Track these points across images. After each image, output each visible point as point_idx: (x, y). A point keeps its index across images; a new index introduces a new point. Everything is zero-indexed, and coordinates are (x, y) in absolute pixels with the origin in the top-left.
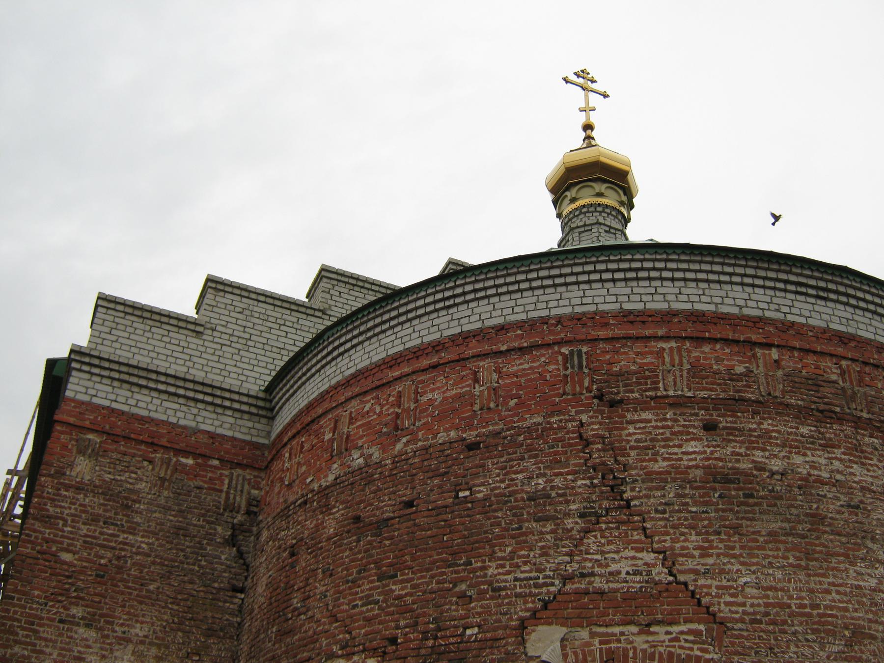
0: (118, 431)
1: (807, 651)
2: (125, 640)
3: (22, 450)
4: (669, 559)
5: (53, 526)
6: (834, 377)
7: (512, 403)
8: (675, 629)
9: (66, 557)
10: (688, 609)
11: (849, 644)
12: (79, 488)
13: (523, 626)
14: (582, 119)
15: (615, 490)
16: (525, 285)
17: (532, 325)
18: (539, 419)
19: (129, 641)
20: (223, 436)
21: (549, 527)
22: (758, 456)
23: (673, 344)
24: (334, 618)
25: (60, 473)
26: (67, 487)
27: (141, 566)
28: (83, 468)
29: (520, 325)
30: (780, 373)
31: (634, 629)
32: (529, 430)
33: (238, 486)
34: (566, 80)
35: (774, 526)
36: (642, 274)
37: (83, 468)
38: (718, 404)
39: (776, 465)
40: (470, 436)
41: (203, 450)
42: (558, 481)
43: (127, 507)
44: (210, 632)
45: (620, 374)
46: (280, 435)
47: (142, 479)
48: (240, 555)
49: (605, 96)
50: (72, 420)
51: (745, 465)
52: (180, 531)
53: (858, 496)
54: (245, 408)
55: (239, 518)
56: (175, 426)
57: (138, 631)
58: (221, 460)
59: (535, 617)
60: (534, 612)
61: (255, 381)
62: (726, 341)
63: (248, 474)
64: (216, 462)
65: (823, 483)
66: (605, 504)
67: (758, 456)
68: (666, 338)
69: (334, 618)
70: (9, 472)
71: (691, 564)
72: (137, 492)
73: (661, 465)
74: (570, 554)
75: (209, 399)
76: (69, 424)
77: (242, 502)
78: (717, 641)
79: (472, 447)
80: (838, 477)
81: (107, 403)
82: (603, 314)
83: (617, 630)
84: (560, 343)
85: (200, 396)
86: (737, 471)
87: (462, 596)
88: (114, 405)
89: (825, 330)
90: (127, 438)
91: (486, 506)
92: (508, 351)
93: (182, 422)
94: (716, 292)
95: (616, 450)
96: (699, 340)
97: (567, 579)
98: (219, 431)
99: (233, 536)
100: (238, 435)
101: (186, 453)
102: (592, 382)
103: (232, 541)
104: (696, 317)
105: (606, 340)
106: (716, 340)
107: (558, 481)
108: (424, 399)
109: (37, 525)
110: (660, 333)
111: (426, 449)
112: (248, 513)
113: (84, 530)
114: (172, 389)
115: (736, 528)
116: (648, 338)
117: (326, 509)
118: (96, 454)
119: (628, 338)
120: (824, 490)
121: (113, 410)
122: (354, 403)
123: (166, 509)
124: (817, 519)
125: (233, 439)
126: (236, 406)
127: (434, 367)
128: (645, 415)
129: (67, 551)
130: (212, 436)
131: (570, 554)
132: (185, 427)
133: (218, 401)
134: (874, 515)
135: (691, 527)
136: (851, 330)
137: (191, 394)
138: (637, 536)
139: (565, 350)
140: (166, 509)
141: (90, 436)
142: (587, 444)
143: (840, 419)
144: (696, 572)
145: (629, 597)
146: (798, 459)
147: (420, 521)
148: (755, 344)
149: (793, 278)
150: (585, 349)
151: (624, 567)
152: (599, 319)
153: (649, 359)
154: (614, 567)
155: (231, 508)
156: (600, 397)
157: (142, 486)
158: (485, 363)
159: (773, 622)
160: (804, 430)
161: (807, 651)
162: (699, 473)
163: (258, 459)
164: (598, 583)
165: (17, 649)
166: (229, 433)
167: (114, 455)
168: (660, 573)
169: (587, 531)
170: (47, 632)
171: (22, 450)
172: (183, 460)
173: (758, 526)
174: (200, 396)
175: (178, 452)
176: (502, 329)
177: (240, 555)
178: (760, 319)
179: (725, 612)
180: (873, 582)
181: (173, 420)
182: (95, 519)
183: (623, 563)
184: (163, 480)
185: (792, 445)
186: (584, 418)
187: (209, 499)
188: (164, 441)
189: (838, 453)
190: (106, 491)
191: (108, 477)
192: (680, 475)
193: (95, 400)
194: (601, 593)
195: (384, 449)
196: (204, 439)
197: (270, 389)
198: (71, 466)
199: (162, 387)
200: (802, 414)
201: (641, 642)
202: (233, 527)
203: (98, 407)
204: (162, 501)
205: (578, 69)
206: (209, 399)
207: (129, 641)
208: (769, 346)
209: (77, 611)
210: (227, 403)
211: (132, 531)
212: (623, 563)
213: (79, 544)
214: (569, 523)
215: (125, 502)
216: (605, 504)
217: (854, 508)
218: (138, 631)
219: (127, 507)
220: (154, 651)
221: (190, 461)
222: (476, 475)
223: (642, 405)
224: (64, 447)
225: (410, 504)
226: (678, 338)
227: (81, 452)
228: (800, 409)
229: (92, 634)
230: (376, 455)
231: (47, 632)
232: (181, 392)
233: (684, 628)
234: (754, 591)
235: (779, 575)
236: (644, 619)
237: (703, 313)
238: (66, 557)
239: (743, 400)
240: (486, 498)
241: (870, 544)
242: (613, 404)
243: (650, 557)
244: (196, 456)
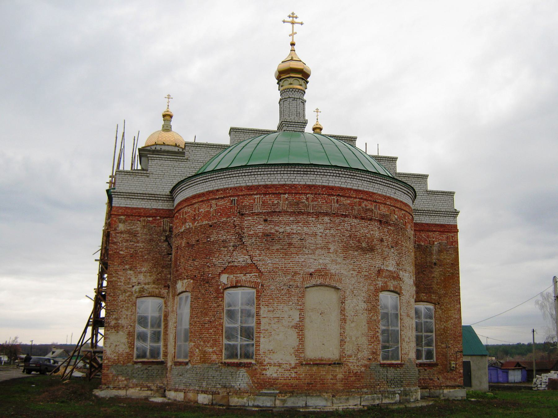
0: (129, 214)
1: (282, 279)
2: (141, 272)
3: (113, 167)
4: (251, 257)
5: (116, 245)
6: (304, 201)
7: (219, 214)
8: (251, 275)
9: (121, 252)
10: (254, 270)
11: (293, 276)
12: (121, 233)
13: (220, 274)
14: (290, 40)
15: (241, 239)
16: (223, 177)
17: (225, 190)
18: (225, 219)
19: (142, 272)
20: (159, 209)
21: (226, 249)
22: (277, 228)
23: (258, 196)
24: (185, 270)
25: (115, 229)
26: (118, 233)
27: (142, 252)
28: (121, 227)
29: (222, 190)
30: (287, 202)
31: (242, 275)
32: (223, 222)
33: (165, 223)
34: (284, 22)
35: (278, 247)
36: (252, 173)
37: (121, 227)
38: (268, 213)
39: (281, 230)
40: (210, 223)
41: (154, 215)
42: (228, 237)
43: (136, 236)
44: (163, 267)
45: (244, 206)
46: (179, 204)
47: (138, 226)
48: (169, 244)
49: (302, 24)
50: (116, 213)
51: (273, 231)
52: (151, 240)
53: (304, 236)
54: (165, 199)
55: (167, 233)
56: (145, 209)
57: (144, 269)
58: (160, 217)
59: (222, 272)
60: (222, 271)
61: (167, 191)
62: (273, 194)
63: (168, 220)
64: (159, 218)
65: (294, 234)
66: (238, 243)
67: (277, 228)
68: (257, 194)
69: (185, 270)
70: (110, 177)
71: (256, 258)
72: (137, 231)
73: (252, 232)
74: (230, 256)
75: (154, 198)
76: (115, 215)
77: (168, 228)
78: (260, 277)
79: (211, 226)
80: (299, 231)
81: (124, 206)
82: (241, 187)
83: (239, 275)
84: (231, 196)
85: (151, 198)
86: (271, 233)
87: (208, 266)
88: (127, 206)
89: (305, 185)
90: (132, 215)
91: (213, 243)
92: (219, 198)
93: (147, 207)
94: (272, 177)
95: (242, 228)
96: (265, 194)
97: (229, 263)
98: (159, 208)
99: (166, 239)
100: (164, 208)
101: (150, 217)
102: (237, 208)
103: (166, 240)
104: (266, 186)
105: (242, 195)
106: (269, 194)
107: (228, 237)
108: (200, 211)
109: (112, 245)
110: (255, 193)
111: (201, 225)
112: (170, 231)
113: (125, 244)
114: (142, 198)
115: (268, 249)
116: (252, 195)
117: (182, 238)
118: (124, 222)
119: (247, 194)
120: (294, 236)
121: (126, 208)
122: (186, 208)
123: (146, 234)
124: (290, 244)
125: (163, 209)
126: (162, 199)
127: (202, 201)
128: (250, 218)
129: (121, 251)
130: (156, 209)
131: (230, 256)
132: (148, 209)
133: (157, 198)
134: (308, 241)
135: (257, 249)
136: (314, 183)
137: (148, 198)
138: (245, 252)
139: (231, 199)
140: (146, 234)
141: (122, 217)
142: (235, 226)
143: (303, 214)
144: (257, 260)
145: (242, 267)
146: (288, 228)
147: (200, 246)
148: (281, 194)
149: (296, 169)
150: (236, 198)
151: (241, 260)
152: (240, 189)
153: (252, 201)
154: (239, 260)
155: (165, 231)
156: (239, 213)
157: (138, 229)
158: (213, 202)
159: (274, 272)
160: (291, 219)
161: (282, 279)
162: (261, 234)
163: (170, 214)
164: (236, 264)
165: (114, 278)
166: (161, 208)
167: (129, 221)
168: (249, 261)
169: (234, 250)
170: (120, 273)
171: (113, 167)
172: (149, 219)
173: (274, 248)
174: (151, 198)
175: (147, 217)
176: (218, 190)
177: (169, 244)
178: (284, 184)
179: (263, 270)
180: (303, 260)
181: (144, 207)
182: (127, 241)
183: (241, 259)
184: (144, 226)
185: (287, 224)
186: (235, 219)
187: (158, 229)
188: (143, 214)
189: (300, 224)
190: (129, 232)
191: (128, 228)
192: (256, 235)
193: (121, 206)
194: (236, 266)
195: (193, 224)
196: (154, 211)
197: (172, 191)
198: (118, 226)
199: (139, 197)
200: (293, 213)
201: (244, 278)
202: (166, 236)
203: (122, 207)
204: (145, 232)
205: (290, 13)
206: (154, 198)
207: (142, 272)
208: (285, 194)
209: (127, 267)
210: (159, 199)
211: (138, 242)
212: (241, 259)
213: (124, 249)
214: (230, 248)
215: (134, 234)
216: (238, 243)
217: (301, 240)
218: (144, 269)
219: (136, 236)
220: (149, 274)
221: (151, 219)
222: (211, 234)
223: (249, 215)
224: (115, 222)
225: (198, 241)
226: (260, 194)
227: (120, 222)
228: (291, 212)
229: (132, 272)
230: (191, 226)
231: (120, 273)
232: (145, 198)
233: (253, 274)
234: (271, 265)
235: (277, 260)
236: (245, 272)
237: (268, 185)
238: (121, 252)
239: (275, 212)
240: (213, 241)
241: (304, 249)
242: (242, 215)
243: (247, 257)
244: (152, 217)
